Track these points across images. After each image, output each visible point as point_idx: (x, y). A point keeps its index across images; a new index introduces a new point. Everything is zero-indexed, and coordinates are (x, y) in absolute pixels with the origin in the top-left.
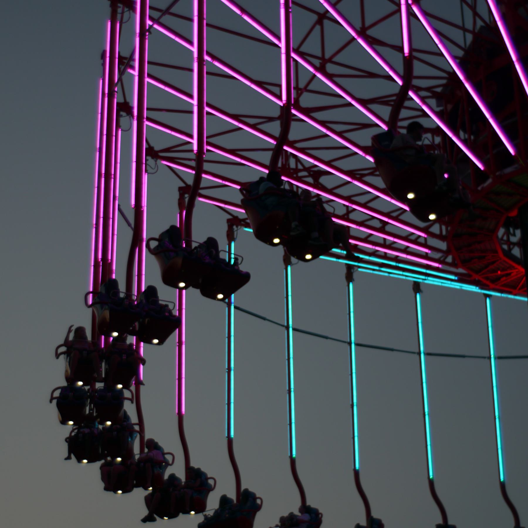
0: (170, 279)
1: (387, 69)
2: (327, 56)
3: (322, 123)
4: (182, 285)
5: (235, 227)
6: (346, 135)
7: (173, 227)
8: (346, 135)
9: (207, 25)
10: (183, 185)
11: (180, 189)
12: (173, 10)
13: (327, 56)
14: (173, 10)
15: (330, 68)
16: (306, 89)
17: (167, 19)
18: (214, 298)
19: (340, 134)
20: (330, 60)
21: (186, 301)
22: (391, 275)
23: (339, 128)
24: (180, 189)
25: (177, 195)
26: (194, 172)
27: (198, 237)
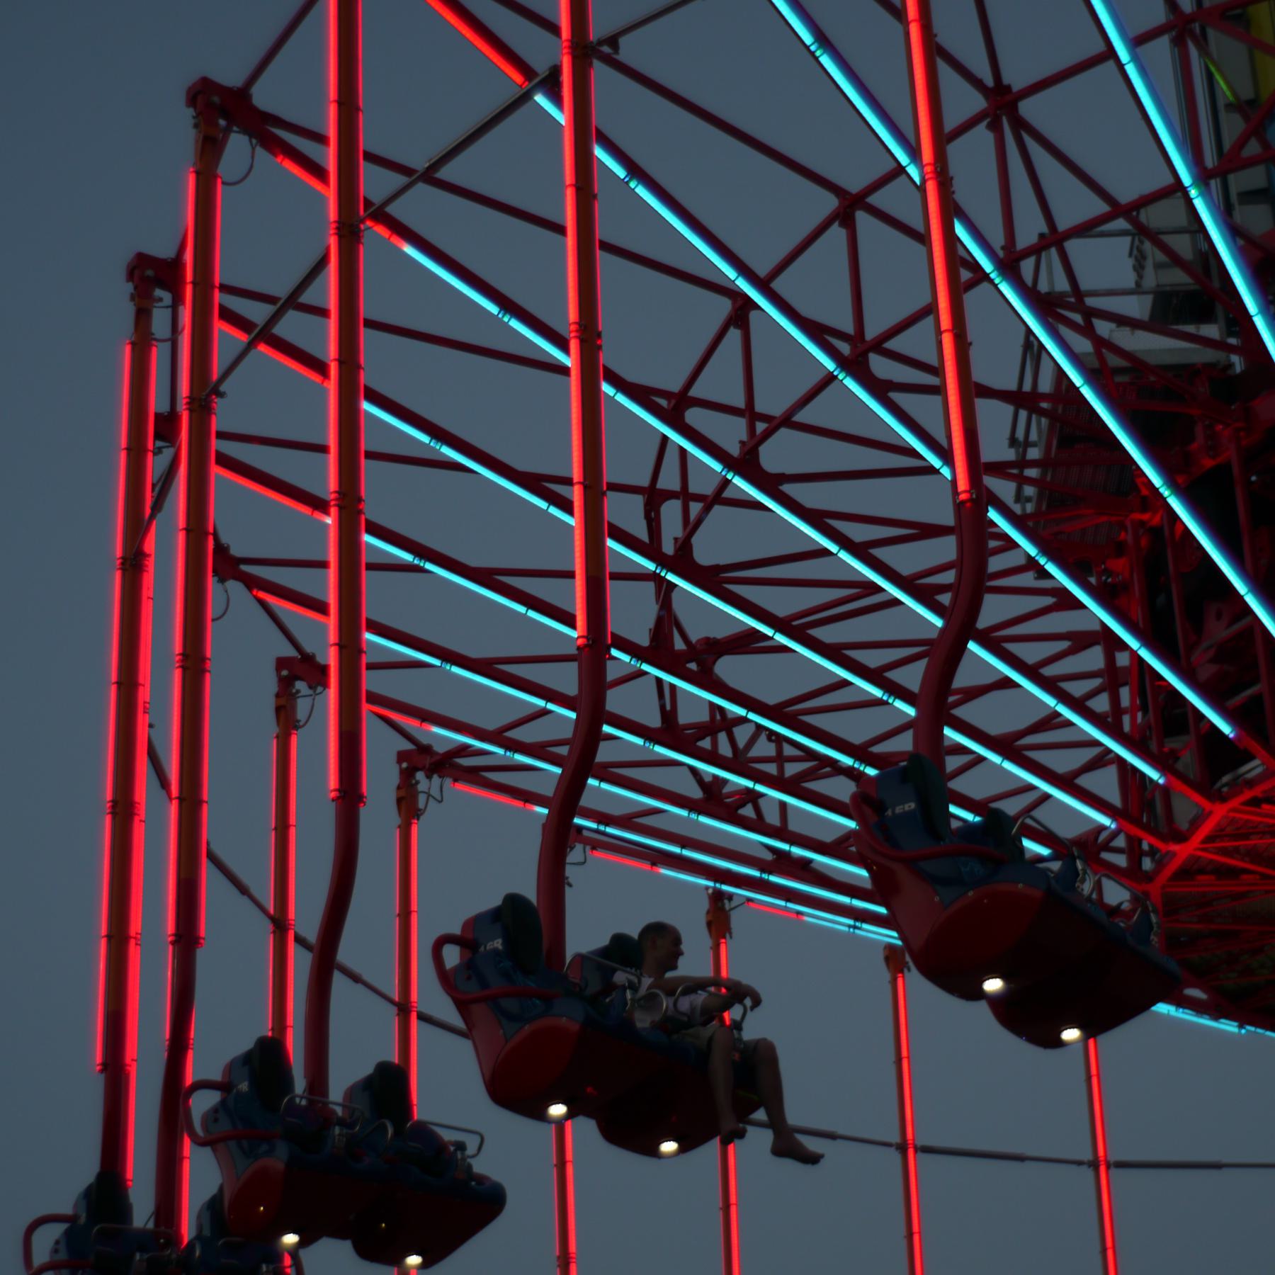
0: (516, 1089)
1: (730, 273)
2: (871, 333)
3: (815, 518)
4: (558, 1110)
5: (420, 775)
6: (878, 552)
7: (514, 902)
8: (878, 552)
9: (561, 230)
10: (291, 652)
11: (281, 663)
12: (444, 173)
13: (871, 333)
14: (444, 173)
15: (880, 366)
16: (787, 421)
17: (880, 366)
18: (654, 1152)
19: (860, 551)
20: (878, 346)
21: (524, 1150)
22: (857, 932)
23: (859, 533)
24: (281, 663)
25: (272, 686)
26: (573, 715)
27: (584, 934)
